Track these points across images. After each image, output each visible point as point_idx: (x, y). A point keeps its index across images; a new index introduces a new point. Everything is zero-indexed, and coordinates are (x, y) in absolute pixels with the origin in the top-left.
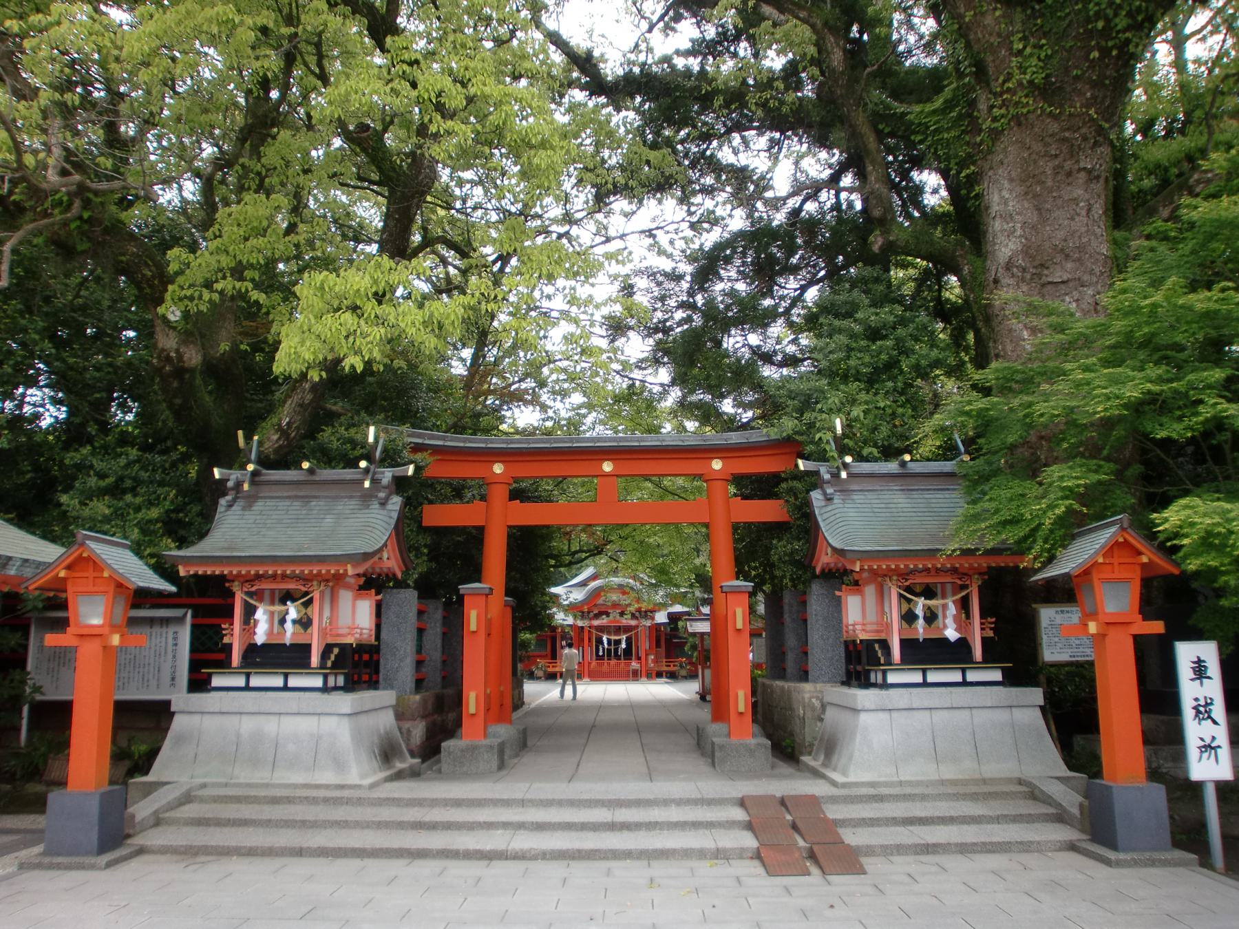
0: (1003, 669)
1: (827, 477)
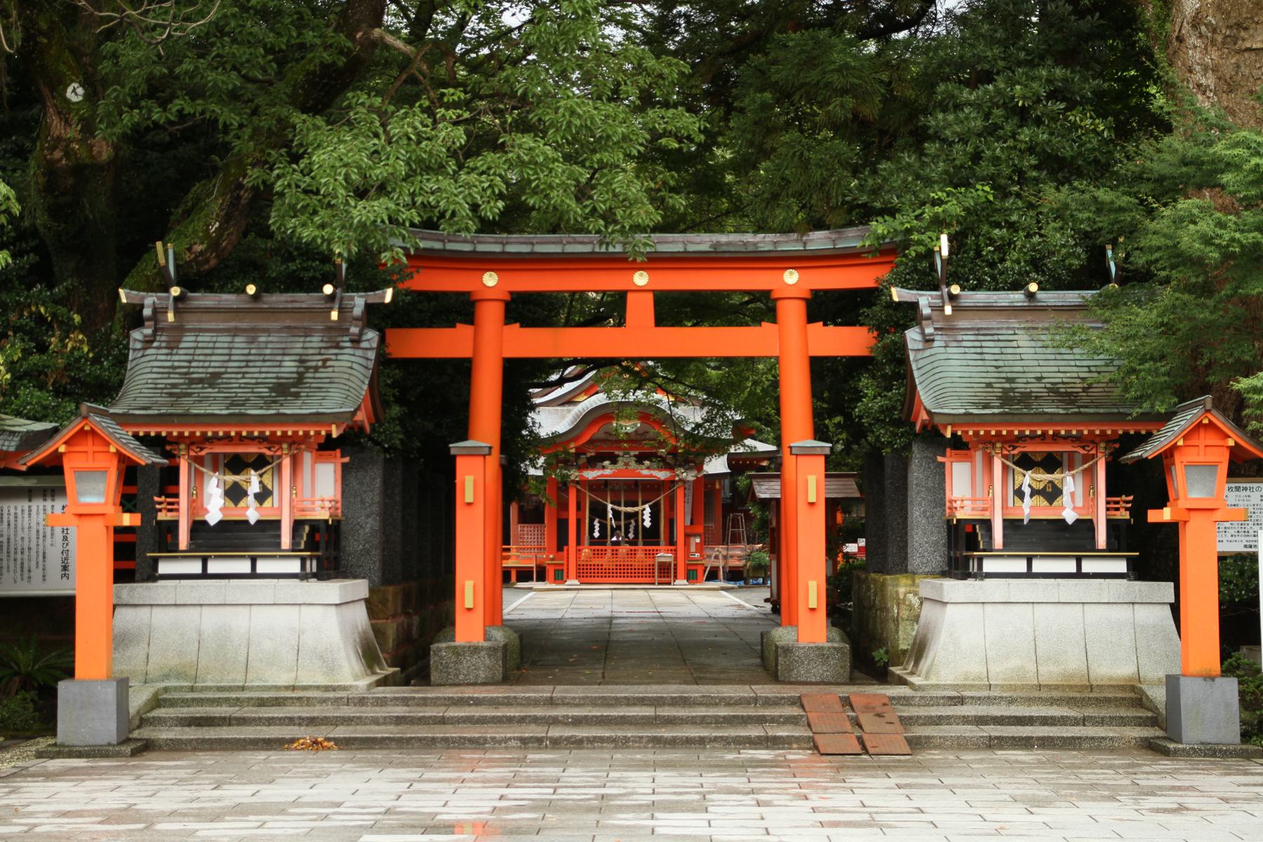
0: (1129, 559)
1: (926, 311)
